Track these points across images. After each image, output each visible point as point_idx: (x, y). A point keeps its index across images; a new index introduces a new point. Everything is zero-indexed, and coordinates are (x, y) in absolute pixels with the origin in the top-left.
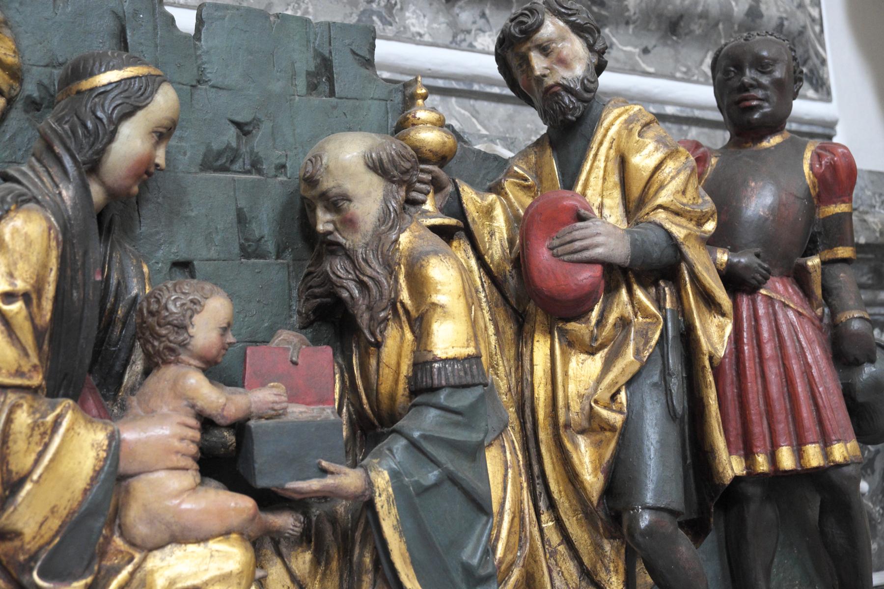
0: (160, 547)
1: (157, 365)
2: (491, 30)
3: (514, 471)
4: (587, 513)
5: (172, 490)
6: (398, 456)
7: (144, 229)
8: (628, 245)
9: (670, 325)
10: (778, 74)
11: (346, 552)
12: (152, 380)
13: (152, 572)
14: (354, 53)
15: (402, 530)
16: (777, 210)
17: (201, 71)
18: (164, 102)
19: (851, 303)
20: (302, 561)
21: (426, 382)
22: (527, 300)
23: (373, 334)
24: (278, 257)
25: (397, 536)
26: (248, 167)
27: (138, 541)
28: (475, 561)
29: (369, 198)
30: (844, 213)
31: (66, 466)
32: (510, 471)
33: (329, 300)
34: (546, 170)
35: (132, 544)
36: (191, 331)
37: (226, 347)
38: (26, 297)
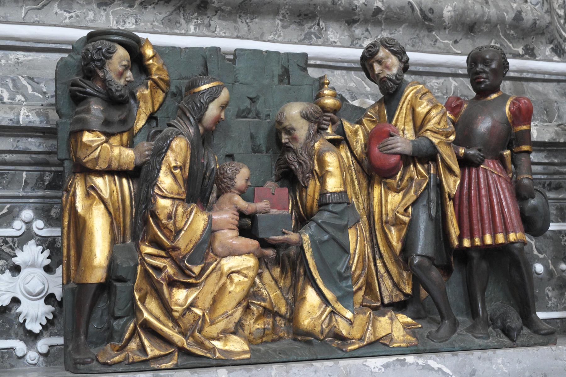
0: (225, 257)
1: (223, 193)
2: (371, 37)
3: (361, 238)
4: (396, 261)
5: (229, 236)
6: (313, 229)
7: (215, 142)
8: (411, 146)
9: (432, 180)
10: (494, 66)
11: (294, 269)
12: (221, 199)
13: (223, 265)
14: (298, 65)
15: (314, 256)
16: (491, 131)
17: (236, 77)
18: (224, 94)
19: (524, 171)
20: (277, 271)
21: (324, 201)
22: (373, 171)
23: (304, 183)
24: (267, 152)
25: (311, 259)
26: (255, 116)
27: (218, 254)
28: (343, 271)
29: (302, 129)
30: (526, 130)
31: (194, 226)
32: (359, 238)
33: (287, 170)
34: (382, 113)
35: (216, 255)
36: (236, 180)
37: (248, 187)
38: (181, 168)
